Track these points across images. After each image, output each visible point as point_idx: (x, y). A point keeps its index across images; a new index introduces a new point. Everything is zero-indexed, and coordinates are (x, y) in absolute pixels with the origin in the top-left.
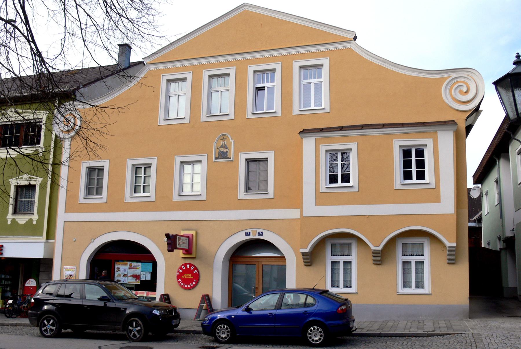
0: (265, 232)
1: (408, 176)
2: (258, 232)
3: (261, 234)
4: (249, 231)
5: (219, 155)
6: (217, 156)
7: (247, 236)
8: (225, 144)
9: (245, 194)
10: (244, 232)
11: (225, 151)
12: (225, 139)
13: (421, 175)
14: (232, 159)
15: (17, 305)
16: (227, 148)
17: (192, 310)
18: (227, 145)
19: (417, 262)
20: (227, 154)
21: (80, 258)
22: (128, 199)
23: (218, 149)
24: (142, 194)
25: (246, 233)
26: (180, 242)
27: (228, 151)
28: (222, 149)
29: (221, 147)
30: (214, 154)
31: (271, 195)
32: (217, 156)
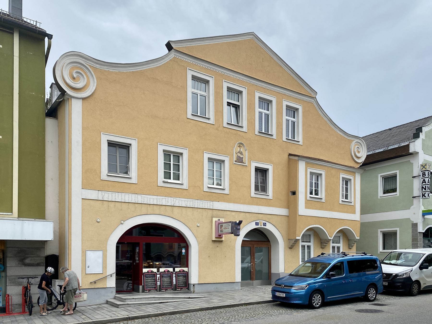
0: (268, 224)
1: (167, 175)
2: (263, 223)
3: (265, 224)
4: (258, 222)
5: (237, 160)
6: (236, 160)
7: (256, 225)
8: (241, 151)
9: (255, 193)
10: (254, 223)
11: (241, 157)
12: (241, 147)
13: (177, 177)
14: (206, 156)
15: (354, 248)
16: (243, 155)
17: (209, 284)
18: (242, 152)
19: (308, 246)
20: (243, 160)
21: (107, 239)
22: (160, 184)
23: (236, 154)
24: (172, 181)
25: (256, 223)
26: (222, 228)
27: (243, 157)
28: (239, 154)
29: (238, 153)
30: (235, 159)
31: (271, 197)
32: (236, 160)
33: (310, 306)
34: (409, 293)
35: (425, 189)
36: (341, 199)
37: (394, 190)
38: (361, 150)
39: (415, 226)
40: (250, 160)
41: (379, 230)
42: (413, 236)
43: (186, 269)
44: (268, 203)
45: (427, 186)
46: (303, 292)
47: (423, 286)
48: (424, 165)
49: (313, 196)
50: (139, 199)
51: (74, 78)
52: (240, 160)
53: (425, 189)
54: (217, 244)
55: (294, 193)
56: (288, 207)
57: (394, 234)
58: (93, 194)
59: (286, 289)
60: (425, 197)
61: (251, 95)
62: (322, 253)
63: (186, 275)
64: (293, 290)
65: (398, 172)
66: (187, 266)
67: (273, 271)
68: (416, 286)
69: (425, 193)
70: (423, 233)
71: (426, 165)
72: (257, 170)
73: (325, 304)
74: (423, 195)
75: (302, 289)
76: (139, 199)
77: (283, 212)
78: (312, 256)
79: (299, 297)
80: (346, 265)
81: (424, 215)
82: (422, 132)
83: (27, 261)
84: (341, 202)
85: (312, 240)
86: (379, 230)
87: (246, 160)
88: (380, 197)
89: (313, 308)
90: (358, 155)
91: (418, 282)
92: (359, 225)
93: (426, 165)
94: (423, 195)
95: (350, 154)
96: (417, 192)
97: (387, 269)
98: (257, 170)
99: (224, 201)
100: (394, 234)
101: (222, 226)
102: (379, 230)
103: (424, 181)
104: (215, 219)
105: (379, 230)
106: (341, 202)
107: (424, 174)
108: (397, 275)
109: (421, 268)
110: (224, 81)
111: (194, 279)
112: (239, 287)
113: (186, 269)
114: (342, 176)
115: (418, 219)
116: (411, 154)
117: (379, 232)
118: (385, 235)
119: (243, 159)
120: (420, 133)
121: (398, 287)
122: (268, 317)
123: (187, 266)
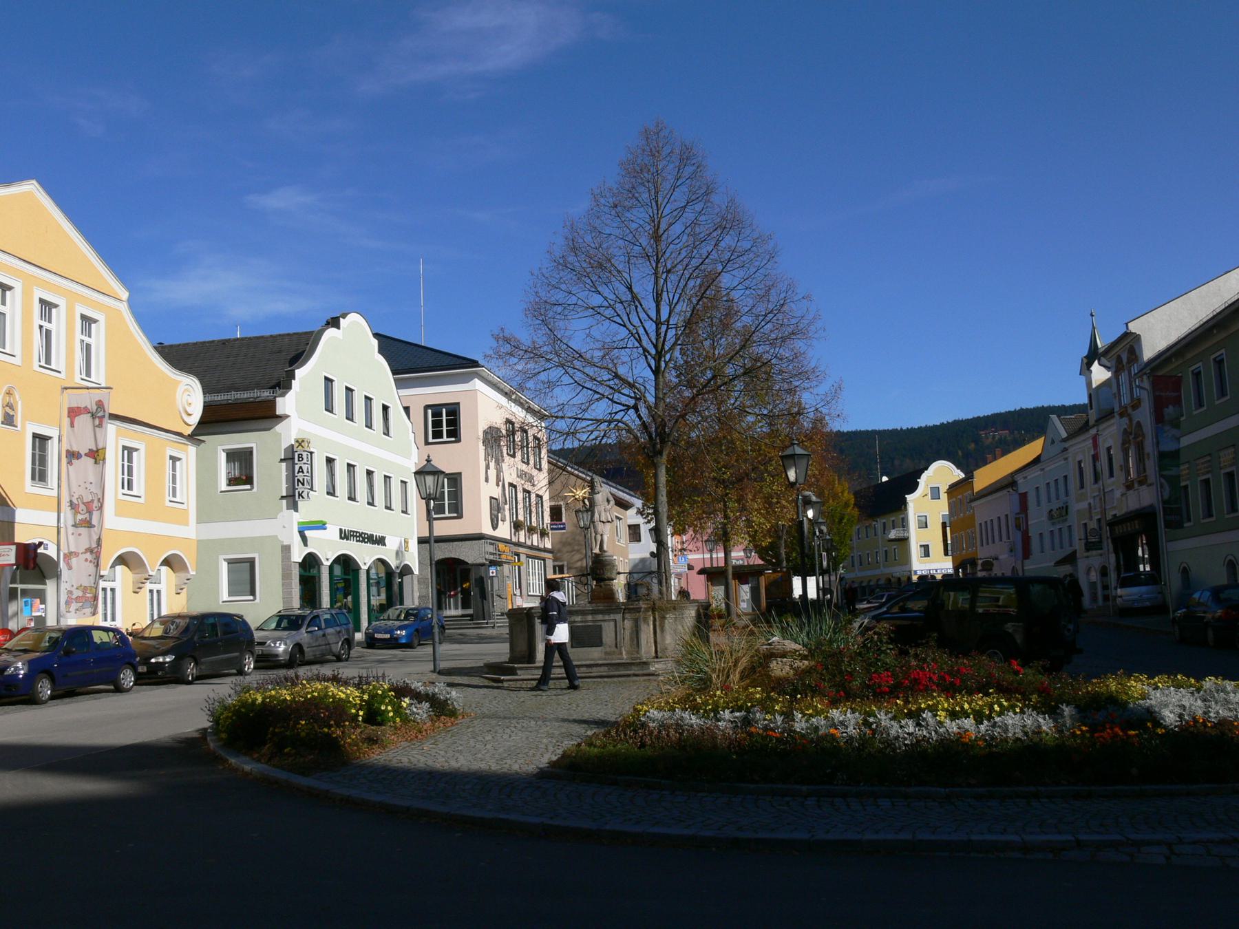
5: (5, 419)
11: (11, 414)
35: (303, 484)
36: (36, 363)
39: (286, 549)
40: (24, 419)
41: (257, 554)
42: (283, 569)
45: (305, 478)
48: (300, 441)
49: (126, 491)
53: (303, 484)
60: (303, 498)
62: (277, 536)
69: (303, 492)
70: (299, 563)
71: (303, 441)
72: (35, 436)
82: (294, 379)
86: (257, 554)
87: (19, 420)
88: (223, 602)
90: (189, 410)
93: (303, 441)
95: (179, 417)
98: (35, 436)
110: (59, 372)
116: (279, 417)
119: (15, 418)
120: (293, 381)
122: (608, 222)
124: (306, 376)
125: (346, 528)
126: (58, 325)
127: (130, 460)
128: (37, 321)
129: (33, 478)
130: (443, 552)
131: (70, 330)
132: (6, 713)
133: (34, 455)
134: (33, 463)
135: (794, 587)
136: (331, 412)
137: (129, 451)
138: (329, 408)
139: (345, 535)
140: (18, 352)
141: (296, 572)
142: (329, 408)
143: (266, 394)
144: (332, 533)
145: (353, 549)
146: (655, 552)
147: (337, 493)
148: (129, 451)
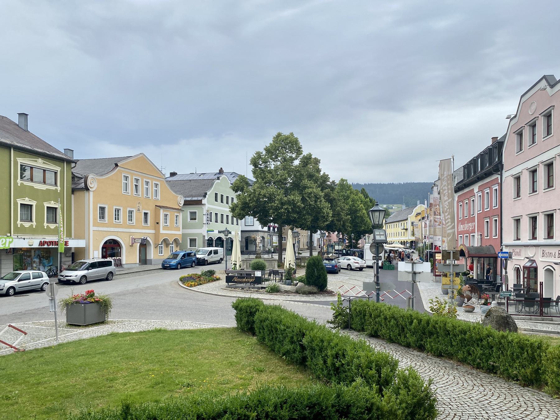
33: (177, 269)
34: (204, 265)
36: (123, 191)
37: (195, 219)
38: (181, 200)
39: (204, 236)
43: (120, 258)
44: (148, 228)
46: (175, 264)
47: (208, 262)
50: (108, 229)
51: (91, 183)
52: (139, 210)
54: (131, 247)
55: (158, 223)
56: (155, 229)
57: (195, 240)
58: (96, 228)
59: (169, 263)
61: (142, 180)
63: (120, 260)
64: (171, 263)
65: (197, 211)
66: (121, 257)
67: (148, 258)
68: (206, 262)
73: (181, 268)
74: (208, 223)
75: (175, 263)
76: (108, 229)
77: (153, 231)
78: (174, 252)
79: (174, 266)
80: (186, 254)
81: (207, 232)
83: (67, 255)
84: (144, 197)
85: (163, 244)
87: (141, 210)
89: (178, 269)
90: (180, 203)
91: (207, 260)
92: (181, 236)
94: (208, 223)
96: (205, 222)
97: (198, 256)
99: (134, 228)
100: (195, 240)
101: (135, 240)
102: (188, 238)
103: (208, 217)
104: (131, 237)
105: (188, 238)
106: (144, 197)
107: (208, 214)
108: (200, 258)
109: (208, 255)
111: (124, 262)
112: (138, 265)
113: (120, 258)
114: (175, 214)
115: (205, 233)
117: (188, 239)
118: (191, 240)
121: (201, 262)
123: (121, 257)
124: (210, 193)
125: (220, 230)
126: (140, 184)
127: (166, 217)
128: (134, 183)
129: (100, 218)
130: (247, 235)
131: (132, 182)
132: (148, 274)
133: (100, 212)
134: (100, 214)
135: (79, 240)
136: (217, 201)
137: (166, 215)
138: (216, 200)
139: (220, 232)
140: (130, 192)
141: (207, 242)
142: (216, 200)
143: (200, 198)
144: (216, 232)
145: (222, 236)
146: (250, 177)
147: (218, 222)
148: (166, 215)
